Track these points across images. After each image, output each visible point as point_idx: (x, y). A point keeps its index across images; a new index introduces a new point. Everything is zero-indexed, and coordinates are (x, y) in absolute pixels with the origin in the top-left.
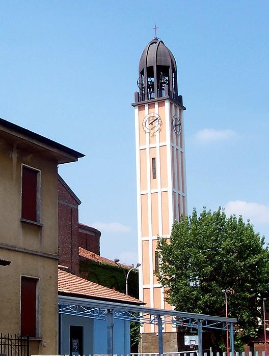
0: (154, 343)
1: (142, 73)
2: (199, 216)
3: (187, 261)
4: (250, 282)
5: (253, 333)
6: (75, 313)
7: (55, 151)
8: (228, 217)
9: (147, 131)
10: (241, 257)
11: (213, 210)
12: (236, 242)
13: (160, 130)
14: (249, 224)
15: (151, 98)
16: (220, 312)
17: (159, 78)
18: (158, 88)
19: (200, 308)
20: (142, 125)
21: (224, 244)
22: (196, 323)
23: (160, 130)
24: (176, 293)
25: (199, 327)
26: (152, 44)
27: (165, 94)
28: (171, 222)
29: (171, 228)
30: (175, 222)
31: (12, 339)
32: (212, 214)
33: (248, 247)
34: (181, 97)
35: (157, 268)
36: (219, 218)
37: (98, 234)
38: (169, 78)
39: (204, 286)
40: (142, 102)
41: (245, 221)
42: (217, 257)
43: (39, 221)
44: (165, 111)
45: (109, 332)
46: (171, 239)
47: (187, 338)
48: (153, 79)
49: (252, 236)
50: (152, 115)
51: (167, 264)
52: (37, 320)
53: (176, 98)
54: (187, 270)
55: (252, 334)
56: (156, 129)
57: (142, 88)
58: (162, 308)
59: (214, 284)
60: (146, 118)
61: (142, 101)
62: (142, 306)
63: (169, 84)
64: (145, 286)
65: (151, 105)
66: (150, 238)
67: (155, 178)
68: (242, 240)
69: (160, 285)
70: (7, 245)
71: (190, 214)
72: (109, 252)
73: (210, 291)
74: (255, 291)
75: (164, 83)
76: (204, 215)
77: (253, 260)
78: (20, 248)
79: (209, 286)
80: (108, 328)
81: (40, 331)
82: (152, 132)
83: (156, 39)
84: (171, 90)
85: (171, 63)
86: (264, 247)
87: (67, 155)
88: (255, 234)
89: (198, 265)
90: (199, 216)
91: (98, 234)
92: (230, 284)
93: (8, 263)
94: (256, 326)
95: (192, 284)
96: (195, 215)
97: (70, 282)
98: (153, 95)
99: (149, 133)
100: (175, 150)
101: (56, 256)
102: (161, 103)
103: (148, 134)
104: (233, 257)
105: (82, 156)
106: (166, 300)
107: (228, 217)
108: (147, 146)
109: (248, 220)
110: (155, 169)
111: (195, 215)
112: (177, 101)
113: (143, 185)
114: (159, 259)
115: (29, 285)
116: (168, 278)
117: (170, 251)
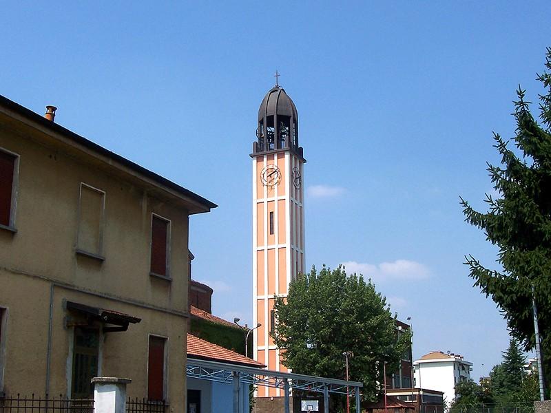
0: (268, 409)
1: (261, 122)
2: (318, 274)
3: (306, 322)
4: (370, 344)
5: (373, 397)
6: (198, 376)
7: (188, 200)
8: (348, 276)
9: (265, 183)
10: (361, 318)
11: (333, 268)
12: (356, 303)
13: (278, 183)
14: (370, 284)
15: (270, 149)
16: (338, 374)
17: (279, 129)
18: (278, 138)
19: (318, 371)
20: (260, 177)
21: (344, 305)
22: (322, 388)
23: (278, 183)
24: (293, 356)
25: (326, 392)
26: (274, 91)
27: (284, 145)
28: (289, 280)
29: (288, 287)
30: (293, 280)
31: (68, 401)
32: (331, 273)
33: (369, 308)
34: (301, 149)
35: (273, 328)
36: (339, 276)
37: (210, 291)
38: (289, 128)
39: (323, 348)
40: (260, 153)
41: (366, 281)
42: (337, 319)
43: (169, 276)
44: (285, 163)
45: (235, 397)
46: (288, 297)
47: (304, 402)
48: (273, 129)
49: (374, 297)
50: (270, 167)
51: (284, 324)
52: (164, 382)
53: (296, 150)
54: (305, 331)
55: (372, 399)
56: (275, 181)
57: (260, 139)
58: (278, 370)
59: (333, 347)
60: (264, 171)
61: (260, 151)
62: (263, 368)
63: (289, 135)
64: (260, 348)
65: (270, 157)
66: (266, 296)
67: (273, 233)
68: (362, 301)
69: (276, 346)
70: (134, 301)
71: (308, 271)
72: (222, 311)
73: (328, 354)
74: (375, 354)
75: (284, 134)
76: (324, 273)
77: (374, 321)
78: (149, 304)
79: (328, 348)
80: (234, 392)
81: (167, 395)
82: (270, 184)
83: (277, 87)
84: (292, 141)
85: (292, 113)
86: (385, 308)
87: (197, 204)
88: (377, 294)
89: (316, 326)
90: (318, 274)
91: (210, 291)
92: (350, 346)
93: (138, 320)
94: (376, 391)
95: (309, 346)
96: (314, 273)
97: (197, 345)
98: (272, 146)
99: (267, 186)
100: (294, 205)
101: (185, 314)
102: (281, 155)
103: (265, 187)
104: (353, 318)
105: (216, 206)
106: (282, 362)
107: (348, 276)
108: (265, 200)
109: (370, 280)
110: (273, 223)
111: (314, 273)
112: (297, 153)
113: (260, 241)
114: (276, 320)
115: (157, 345)
116: (285, 339)
117: (288, 311)
